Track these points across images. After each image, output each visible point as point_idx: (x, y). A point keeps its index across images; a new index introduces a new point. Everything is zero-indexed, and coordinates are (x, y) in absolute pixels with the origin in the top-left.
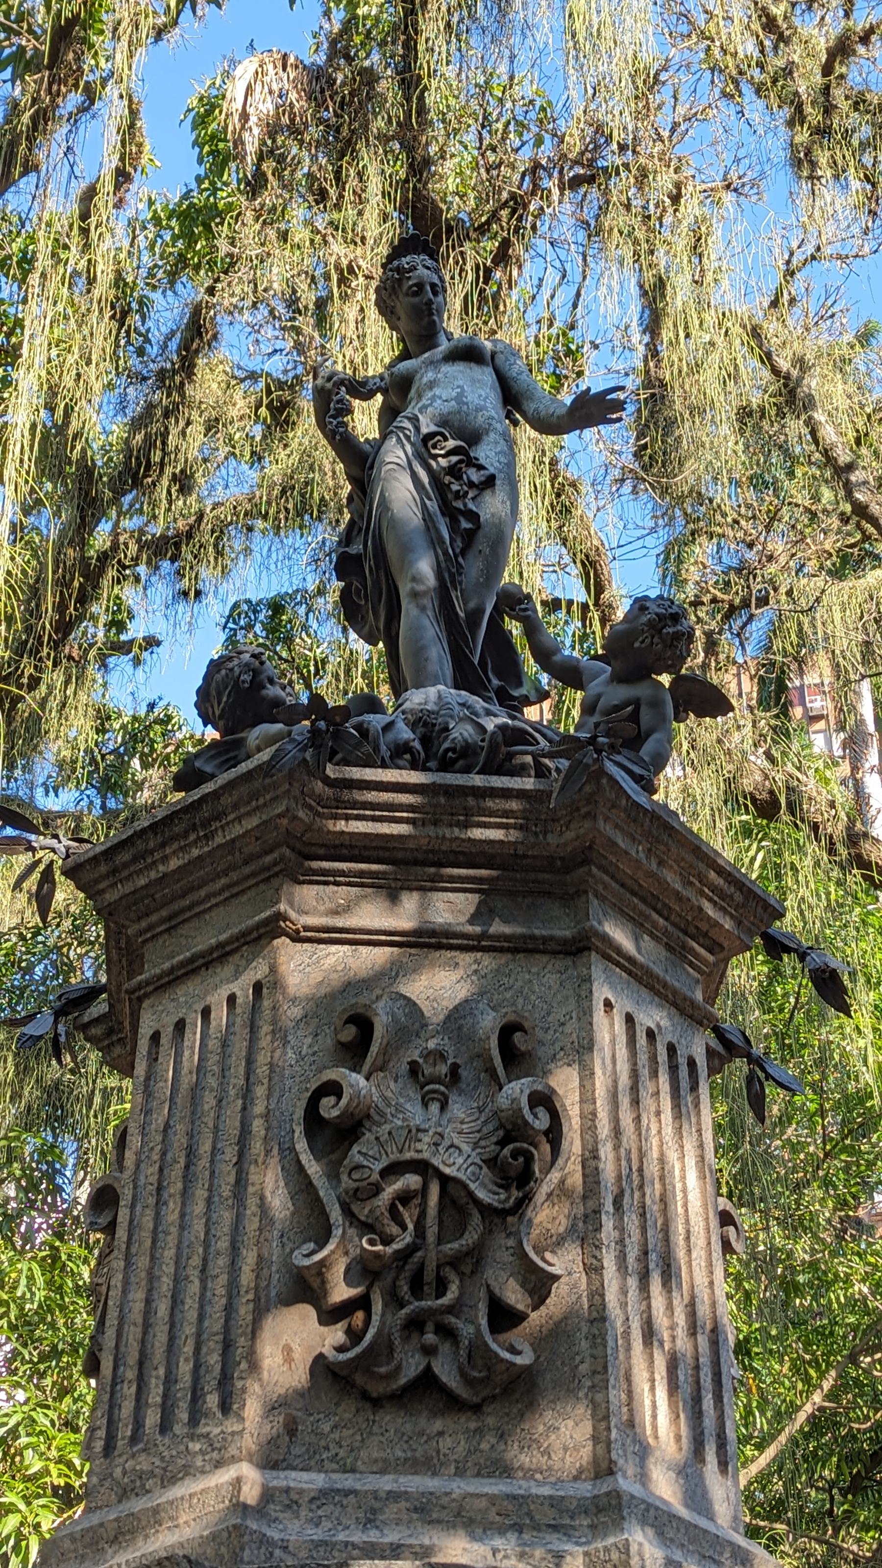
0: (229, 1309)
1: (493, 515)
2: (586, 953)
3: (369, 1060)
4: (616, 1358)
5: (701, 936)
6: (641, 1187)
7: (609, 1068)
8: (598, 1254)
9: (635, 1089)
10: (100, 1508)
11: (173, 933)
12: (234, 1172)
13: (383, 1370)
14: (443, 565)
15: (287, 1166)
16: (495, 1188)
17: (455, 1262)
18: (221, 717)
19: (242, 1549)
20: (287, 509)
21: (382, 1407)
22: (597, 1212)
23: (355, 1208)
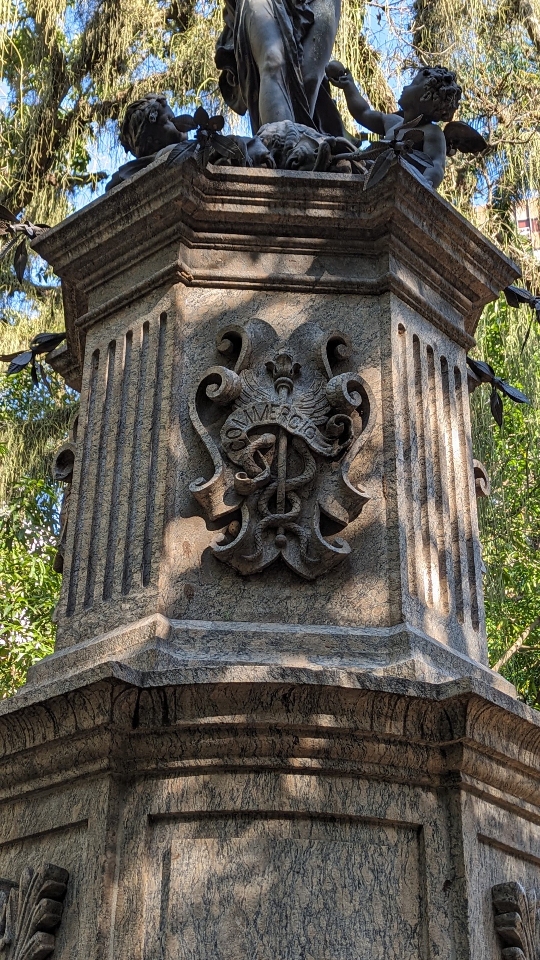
0: (148, 520)
1: (323, 14)
2: (387, 294)
3: (239, 362)
4: (406, 551)
5: (464, 288)
6: (423, 446)
7: (402, 370)
8: (393, 486)
9: (418, 381)
10: (65, 647)
11: (107, 286)
12: (149, 435)
13: (250, 557)
14: (289, 49)
15: (185, 430)
16: (324, 443)
17: (298, 490)
18: (137, 144)
19: (157, 665)
20: (187, 83)
21: (250, 581)
22: (393, 459)
23: (231, 455)
